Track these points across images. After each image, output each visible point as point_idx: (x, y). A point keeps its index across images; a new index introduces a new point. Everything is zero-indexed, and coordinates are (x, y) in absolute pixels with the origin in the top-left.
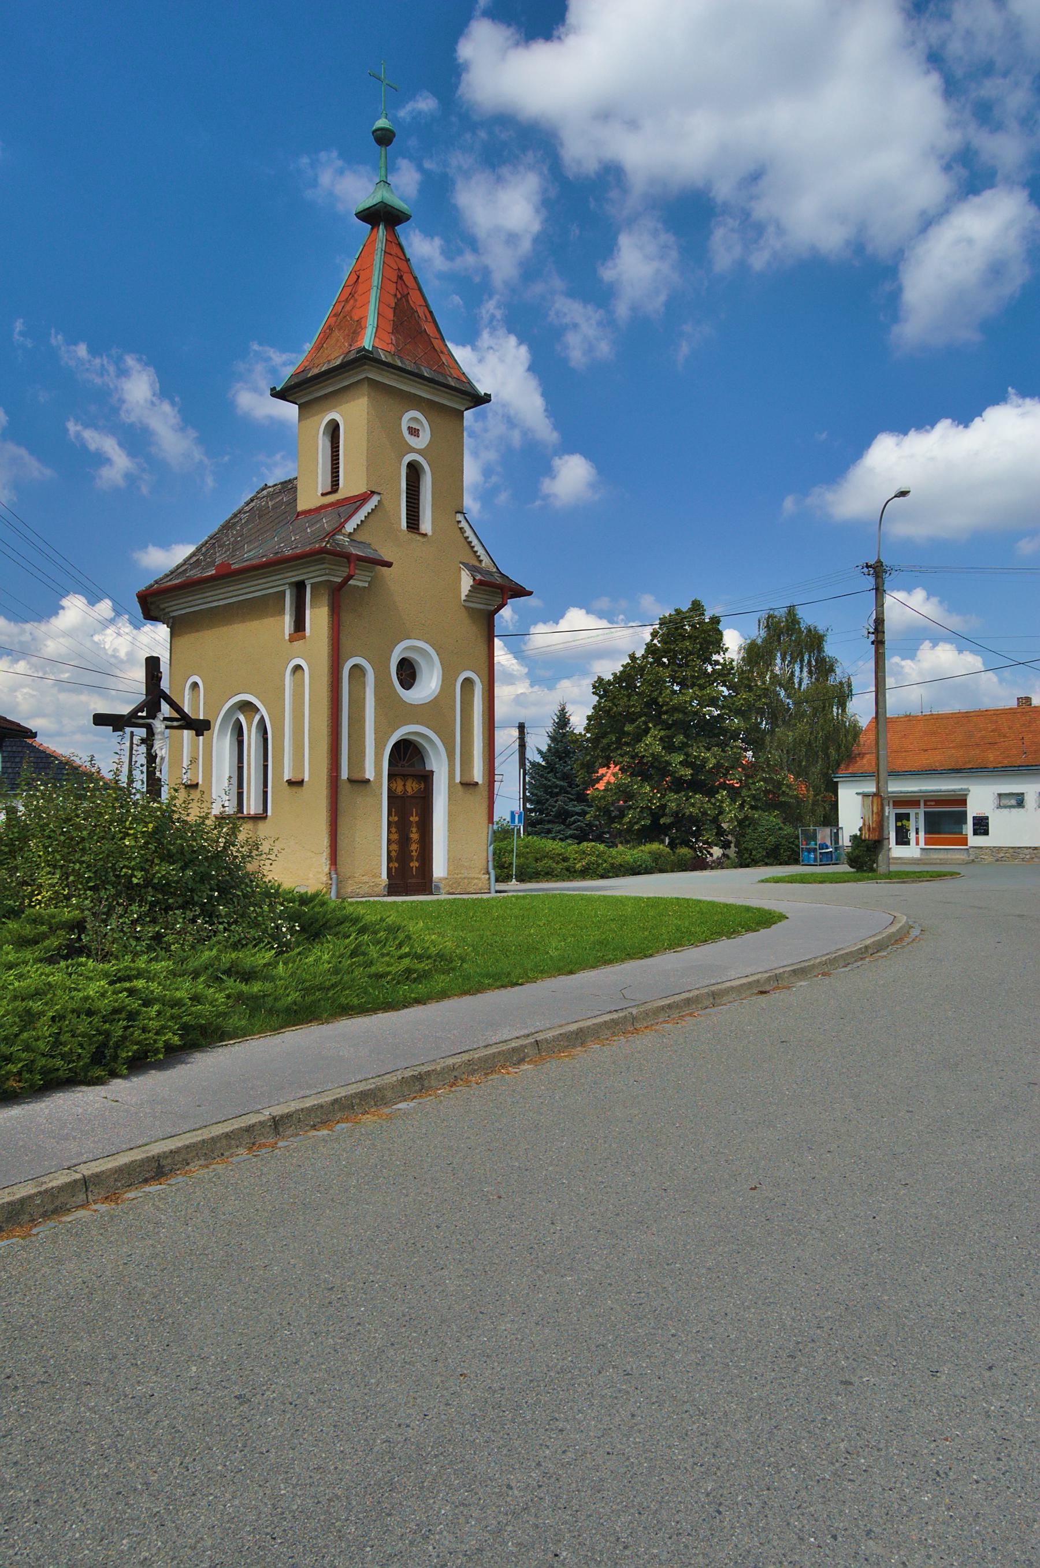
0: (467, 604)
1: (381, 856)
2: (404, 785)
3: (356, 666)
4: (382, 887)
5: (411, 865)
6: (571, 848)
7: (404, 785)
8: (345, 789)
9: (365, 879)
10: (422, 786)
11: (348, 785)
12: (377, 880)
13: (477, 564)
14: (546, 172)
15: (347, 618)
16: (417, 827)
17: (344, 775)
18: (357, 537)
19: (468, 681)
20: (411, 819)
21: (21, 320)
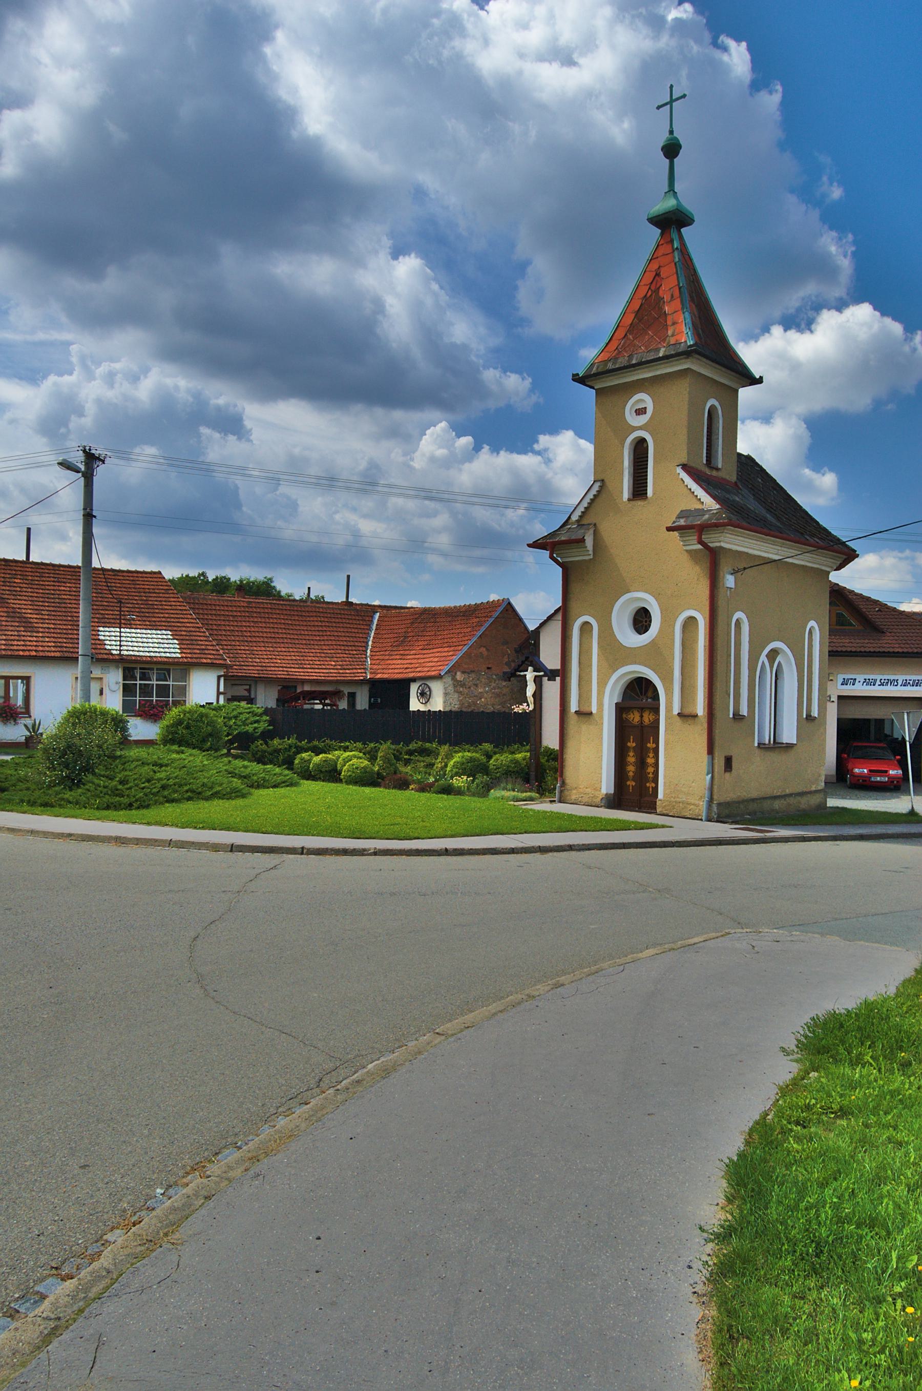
0: (685, 548)
1: (665, 776)
2: (642, 716)
3: (586, 623)
4: (599, 799)
5: (648, 785)
6: (255, 767)
7: (642, 716)
8: (572, 720)
9: (589, 790)
10: (624, 716)
11: (575, 717)
12: (596, 793)
13: (699, 506)
14: (239, 481)
15: (575, 588)
16: (634, 751)
17: (573, 707)
18: (585, 522)
19: (691, 620)
20: (649, 745)
21: (541, 400)
